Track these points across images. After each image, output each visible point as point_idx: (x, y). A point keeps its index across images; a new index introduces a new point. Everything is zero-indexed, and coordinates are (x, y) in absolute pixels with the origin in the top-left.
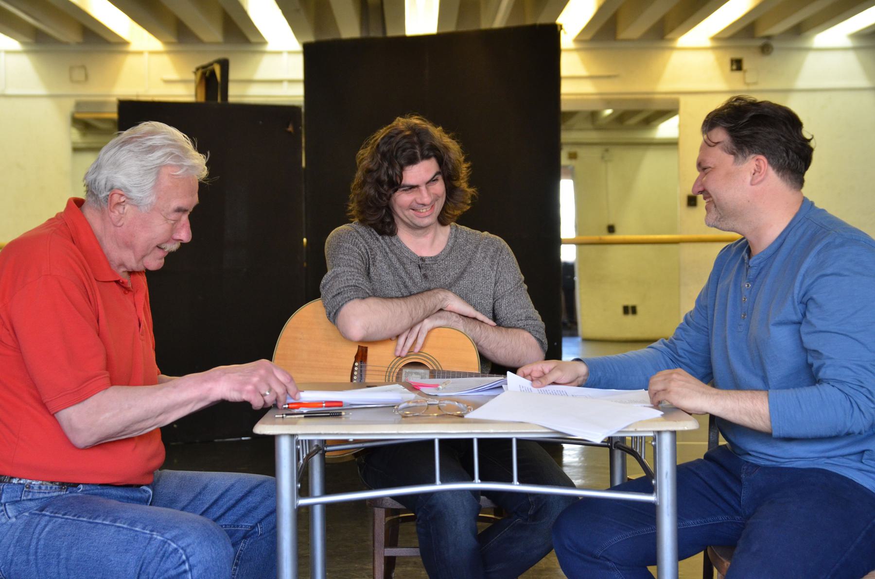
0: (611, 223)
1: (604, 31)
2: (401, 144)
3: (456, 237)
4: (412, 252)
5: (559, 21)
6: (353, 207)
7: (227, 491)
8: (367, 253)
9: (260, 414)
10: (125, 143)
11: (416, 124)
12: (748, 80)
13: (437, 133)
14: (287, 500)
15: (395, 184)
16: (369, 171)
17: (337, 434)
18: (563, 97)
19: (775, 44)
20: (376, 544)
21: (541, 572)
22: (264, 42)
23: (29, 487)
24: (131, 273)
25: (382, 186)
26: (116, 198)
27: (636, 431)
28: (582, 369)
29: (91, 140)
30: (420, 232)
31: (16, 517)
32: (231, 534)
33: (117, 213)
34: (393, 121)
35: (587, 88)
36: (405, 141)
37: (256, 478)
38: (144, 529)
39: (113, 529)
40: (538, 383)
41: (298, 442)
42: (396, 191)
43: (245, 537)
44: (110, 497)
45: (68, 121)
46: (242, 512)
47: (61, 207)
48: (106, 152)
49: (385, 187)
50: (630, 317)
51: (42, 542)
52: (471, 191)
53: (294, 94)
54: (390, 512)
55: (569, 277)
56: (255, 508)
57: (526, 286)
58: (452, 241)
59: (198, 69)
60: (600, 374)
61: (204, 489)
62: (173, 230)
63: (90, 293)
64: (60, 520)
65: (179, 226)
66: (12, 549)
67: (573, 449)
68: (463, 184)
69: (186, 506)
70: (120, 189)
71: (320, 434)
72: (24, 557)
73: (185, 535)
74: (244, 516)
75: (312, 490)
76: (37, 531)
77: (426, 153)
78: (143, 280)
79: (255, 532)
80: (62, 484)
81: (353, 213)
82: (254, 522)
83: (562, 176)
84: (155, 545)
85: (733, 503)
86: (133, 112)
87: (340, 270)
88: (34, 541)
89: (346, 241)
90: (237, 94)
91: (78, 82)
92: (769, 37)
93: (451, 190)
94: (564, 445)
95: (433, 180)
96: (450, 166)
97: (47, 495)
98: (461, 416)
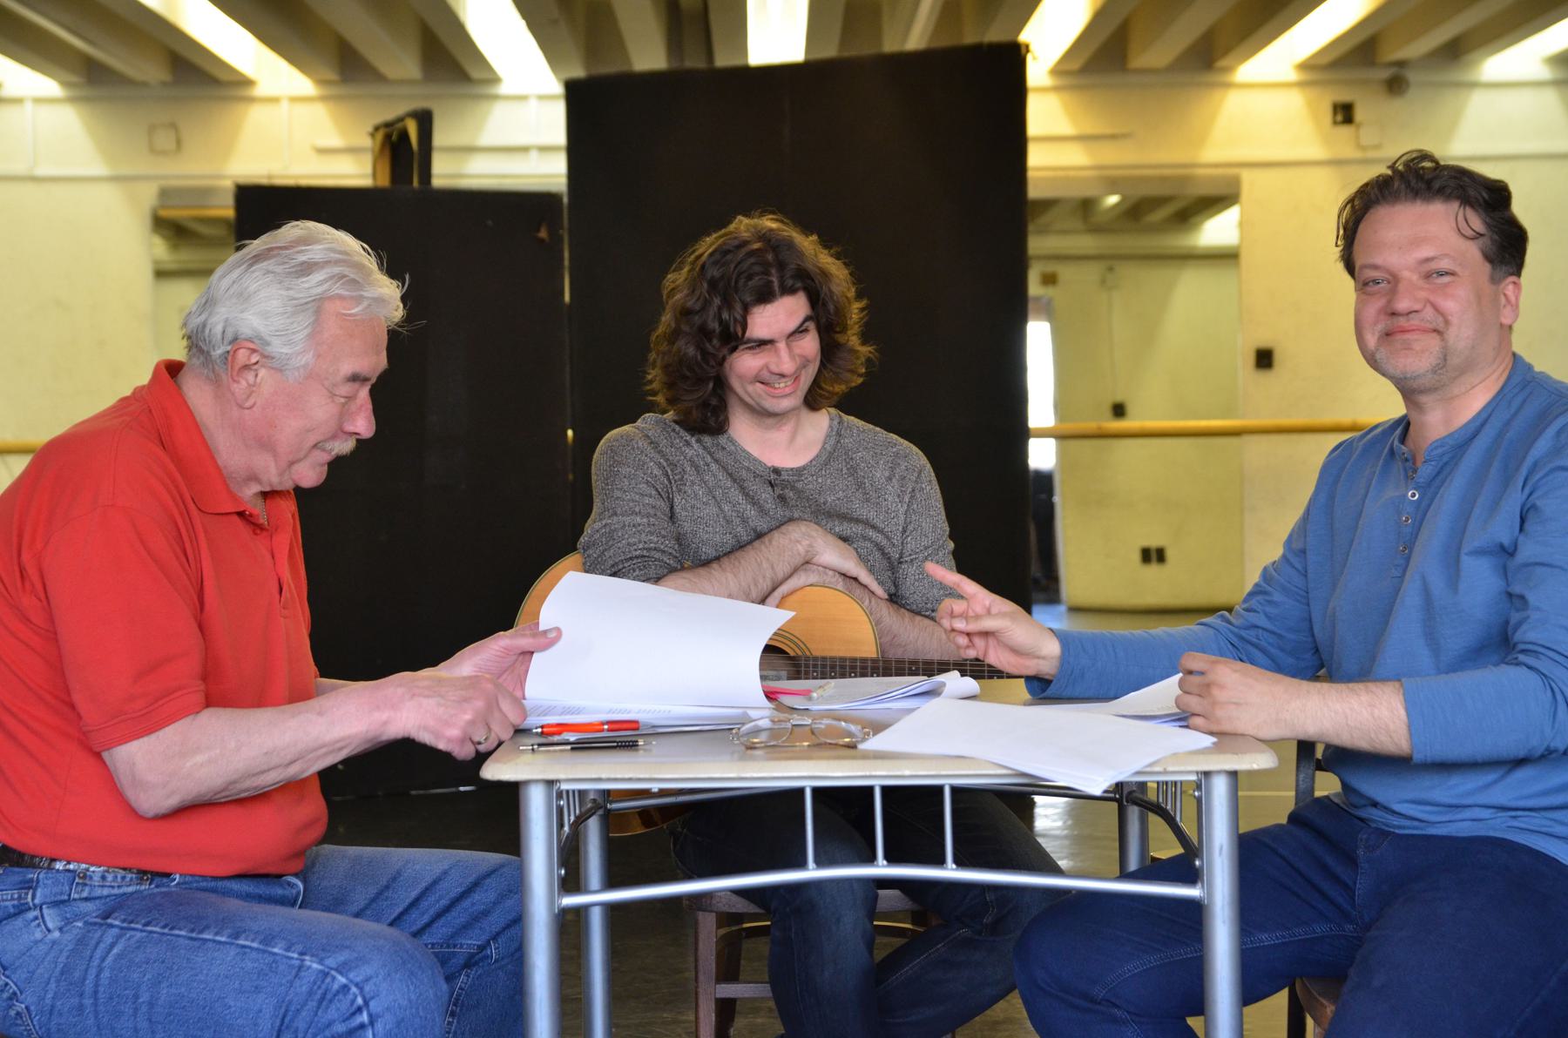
0: (1119, 398)
1: (1103, 56)
2: (745, 265)
3: (839, 434)
4: (755, 459)
5: (1023, 37)
6: (655, 376)
7: (435, 882)
9: (481, 758)
10: (257, 258)
11: (771, 230)
13: (807, 244)
14: (541, 898)
15: (734, 338)
16: (685, 313)
17: (630, 780)
18: (1031, 174)
19: (1412, 76)
20: (701, 978)
21: (995, 1025)
22: (494, 80)
23: (85, 877)
25: (710, 341)
26: (242, 356)
27: (1165, 772)
29: (189, 256)
30: (770, 421)
31: (61, 929)
32: (443, 960)
33: (244, 383)
34: (730, 222)
35: (1074, 158)
36: (752, 260)
38: (288, 949)
39: (233, 951)
41: (560, 795)
42: (734, 349)
43: (469, 964)
44: (227, 893)
45: (148, 222)
47: (144, 378)
48: (223, 276)
49: (715, 341)
50: (1154, 569)
51: (106, 974)
52: (865, 350)
54: (728, 918)
56: (485, 913)
58: (832, 441)
59: (377, 129)
61: (394, 879)
62: (344, 414)
64: (139, 935)
65: (353, 407)
66: (53, 985)
68: (853, 339)
69: (366, 908)
70: (250, 340)
71: (599, 780)
73: (362, 960)
74: (466, 927)
77: (790, 282)
78: (289, 508)
80: (142, 873)
81: (655, 385)
82: (484, 938)
83: (1030, 315)
85: (1340, 900)
86: (264, 208)
88: (93, 972)
90: (448, 171)
91: (164, 153)
92: (1401, 64)
93: (830, 350)
94: (1037, 798)
95: (800, 331)
96: (831, 307)
97: (116, 891)
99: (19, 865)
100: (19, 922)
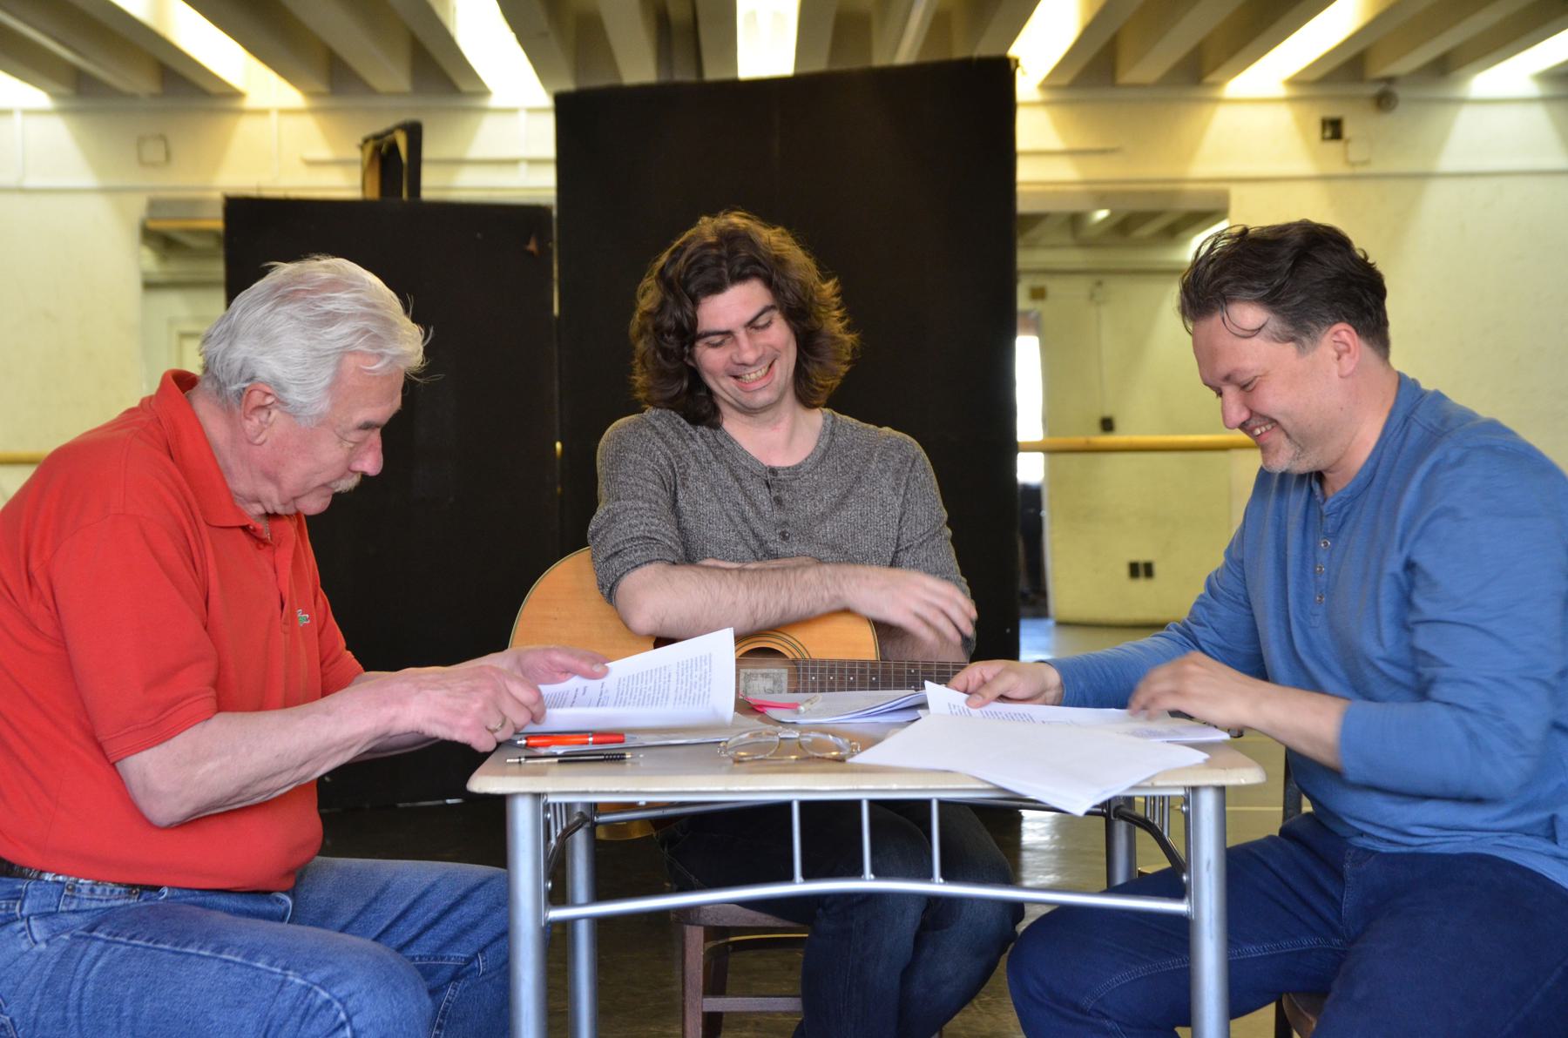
0: (1107, 413)
1: (1094, 69)
3: (833, 433)
5: (1013, 52)
7: (424, 894)
8: (671, 466)
12: (1353, 157)
13: (773, 238)
14: (528, 911)
17: (617, 793)
18: (1020, 189)
19: (1401, 92)
20: (688, 991)
22: (484, 92)
23: (74, 889)
24: (272, 516)
26: (257, 398)
27: (1153, 787)
28: (1053, 677)
29: (177, 268)
31: (47, 941)
32: (427, 972)
35: (1064, 172)
37: (480, 871)
38: (271, 964)
39: (216, 965)
40: (978, 699)
41: (547, 808)
43: (455, 977)
45: (136, 234)
46: (450, 932)
51: (90, 987)
53: (536, 182)
55: (1032, 511)
56: (474, 926)
57: (949, 532)
58: (826, 440)
59: (366, 141)
60: (1081, 684)
61: (383, 891)
63: (194, 548)
64: (123, 948)
66: (37, 998)
67: (1040, 820)
70: (267, 384)
72: (59, 1014)
73: (344, 976)
74: (454, 939)
75: (573, 895)
76: (83, 967)
78: (291, 528)
79: (474, 969)
82: (472, 950)
83: (1019, 330)
84: (291, 992)
87: (625, 504)
89: (634, 447)
90: (437, 184)
91: (153, 165)
92: (1390, 80)
94: (1025, 813)
97: (104, 905)
98: (841, 760)
99: (8, 875)
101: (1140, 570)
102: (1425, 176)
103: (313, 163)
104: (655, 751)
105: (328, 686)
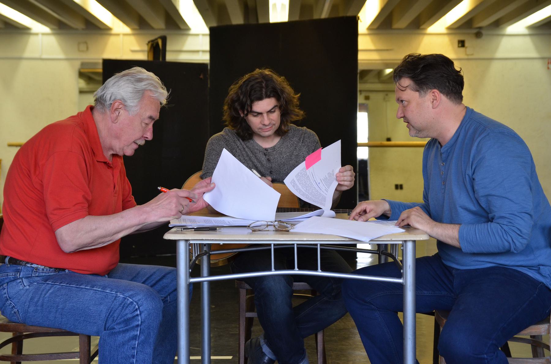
1: (384, 23)
7: (151, 276)
12: (468, 53)
13: (279, 80)
18: (359, 62)
19: (484, 32)
22: (188, 29)
31: (29, 286)
35: (375, 56)
39: (92, 292)
41: (190, 245)
45: (75, 75)
50: (399, 191)
53: (205, 58)
59: (149, 42)
61: (138, 274)
64: (58, 286)
73: (137, 294)
76: (44, 293)
78: (120, 162)
80: (56, 269)
82: (167, 294)
86: (113, 67)
91: (83, 51)
92: (480, 28)
97: (47, 274)
99: (15, 264)
100: (14, 283)
101: (399, 187)
102: (492, 59)
103: (133, 51)
104: (484, 250)
105: (125, 206)
